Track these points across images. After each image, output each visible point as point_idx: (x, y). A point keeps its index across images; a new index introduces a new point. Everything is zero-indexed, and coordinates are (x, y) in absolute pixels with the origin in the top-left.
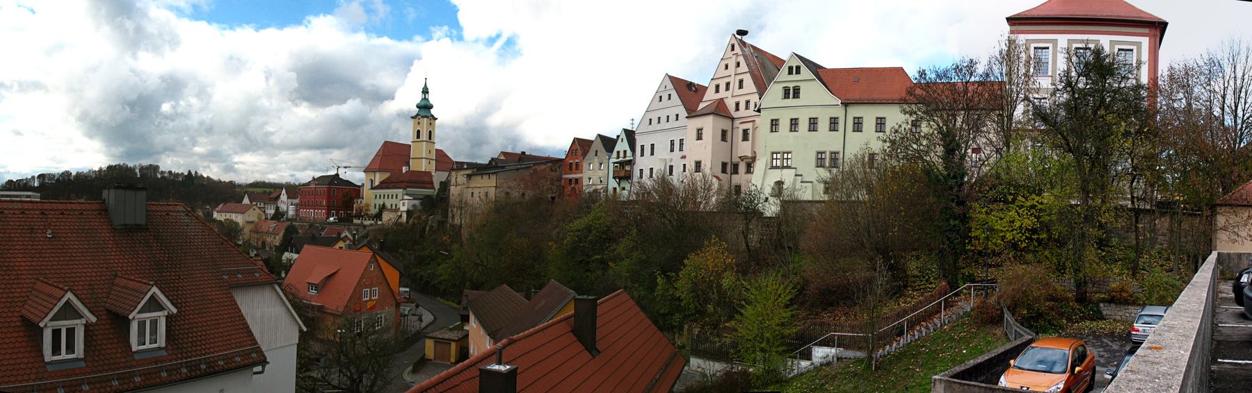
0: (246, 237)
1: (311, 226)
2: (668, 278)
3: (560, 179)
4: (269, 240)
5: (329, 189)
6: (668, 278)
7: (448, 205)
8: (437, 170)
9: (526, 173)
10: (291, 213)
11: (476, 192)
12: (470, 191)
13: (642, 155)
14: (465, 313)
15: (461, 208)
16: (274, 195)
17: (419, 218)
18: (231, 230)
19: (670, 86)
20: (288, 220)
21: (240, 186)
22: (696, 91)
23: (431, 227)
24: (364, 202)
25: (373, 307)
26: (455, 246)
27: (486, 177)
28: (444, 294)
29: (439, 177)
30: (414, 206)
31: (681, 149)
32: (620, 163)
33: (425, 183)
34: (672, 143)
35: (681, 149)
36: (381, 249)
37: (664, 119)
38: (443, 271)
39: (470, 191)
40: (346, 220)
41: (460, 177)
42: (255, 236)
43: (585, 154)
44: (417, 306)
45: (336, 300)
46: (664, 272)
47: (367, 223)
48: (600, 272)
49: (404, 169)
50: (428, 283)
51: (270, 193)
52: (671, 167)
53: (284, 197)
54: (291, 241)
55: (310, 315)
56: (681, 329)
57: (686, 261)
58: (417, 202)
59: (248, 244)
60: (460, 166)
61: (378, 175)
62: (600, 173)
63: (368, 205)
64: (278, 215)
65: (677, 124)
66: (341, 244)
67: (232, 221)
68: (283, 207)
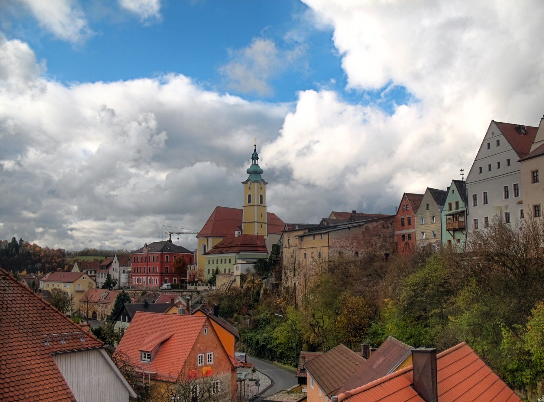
0: (76, 307)
1: (144, 294)
2: (514, 329)
3: (392, 236)
4: (99, 309)
5: (162, 255)
6: (514, 329)
7: (281, 267)
8: (269, 233)
9: (358, 231)
10: (123, 281)
11: (309, 252)
12: (303, 252)
13: (475, 204)
14: (302, 375)
15: (295, 270)
16: (105, 263)
17: (253, 281)
18: (60, 302)
19: (497, 132)
20: (120, 288)
21: (69, 254)
22: (526, 133)
23: (266, 290)
24: (197, 267)
25: (208, 373)
26: (290, 309)
27: (318, 237)
28: (281, 358)
29: (271, 241)
30: (247, 270)
31: (516, 195)
32: (453, 215)
33: (257, 246)
34: (506, 188)
35: (516, 195)
36: (216, 314)
37: (494, 166)
38: (279, 334)
39: (303, 252)
40: (180, 286)
41: (292, 239)
42: (85, 306)
43: (416, 209)
44: (254, 371)
45: (170, 366)
46: (509, 324)
47: (201, 288)
48: (440, 327)
49: (237, 234)
50: (264, 347)
51: (101, 262)
52: (507, 215)
53: (116, 265)
54: (122, 311)
55: (142, 383)
56: (534, 386)
57: (533, 311)
58: (251, 266)
59: (78, 315)
60: (292, 228)
61: (210, 240)
62: (433, 227)
63: (201, 271)
64: (109, 284)
65: (509, 169)
66: (174, 310)
67: (60, 291)
68: (115, 275)
